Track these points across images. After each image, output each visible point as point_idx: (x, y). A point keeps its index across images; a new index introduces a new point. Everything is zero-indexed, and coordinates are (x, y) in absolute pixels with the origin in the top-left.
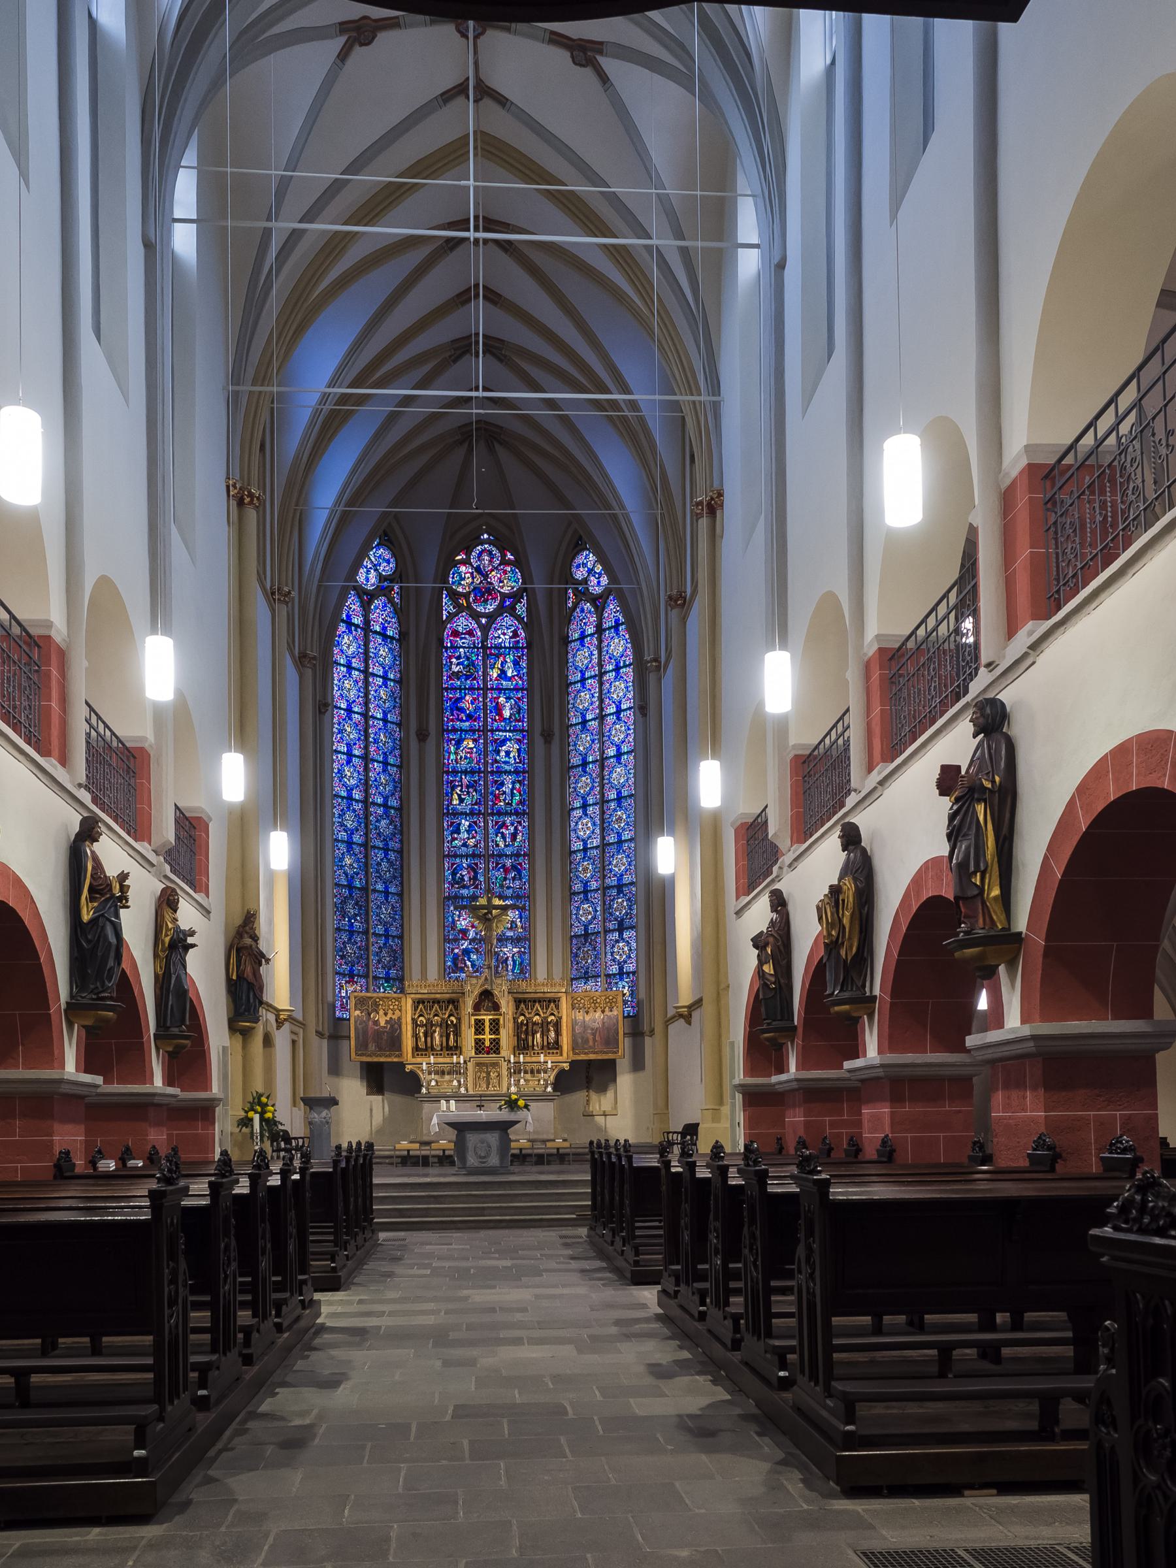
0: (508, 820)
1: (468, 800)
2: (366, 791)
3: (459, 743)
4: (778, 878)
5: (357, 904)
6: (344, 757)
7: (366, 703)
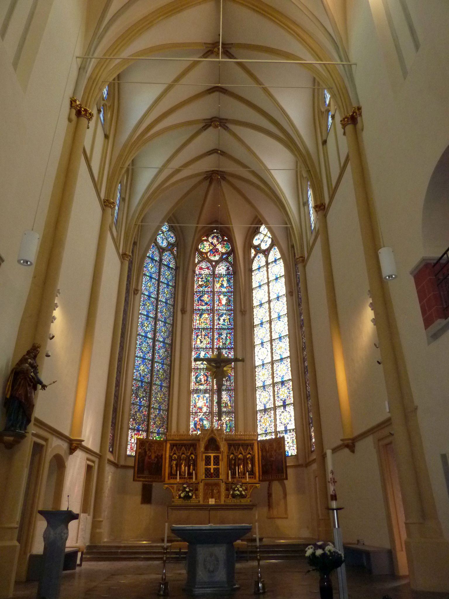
1: (205, 342)
2: (155, 334)
3: (201, 316)
5: (144, 391)
6: (145, 317)
7: (158, 294)
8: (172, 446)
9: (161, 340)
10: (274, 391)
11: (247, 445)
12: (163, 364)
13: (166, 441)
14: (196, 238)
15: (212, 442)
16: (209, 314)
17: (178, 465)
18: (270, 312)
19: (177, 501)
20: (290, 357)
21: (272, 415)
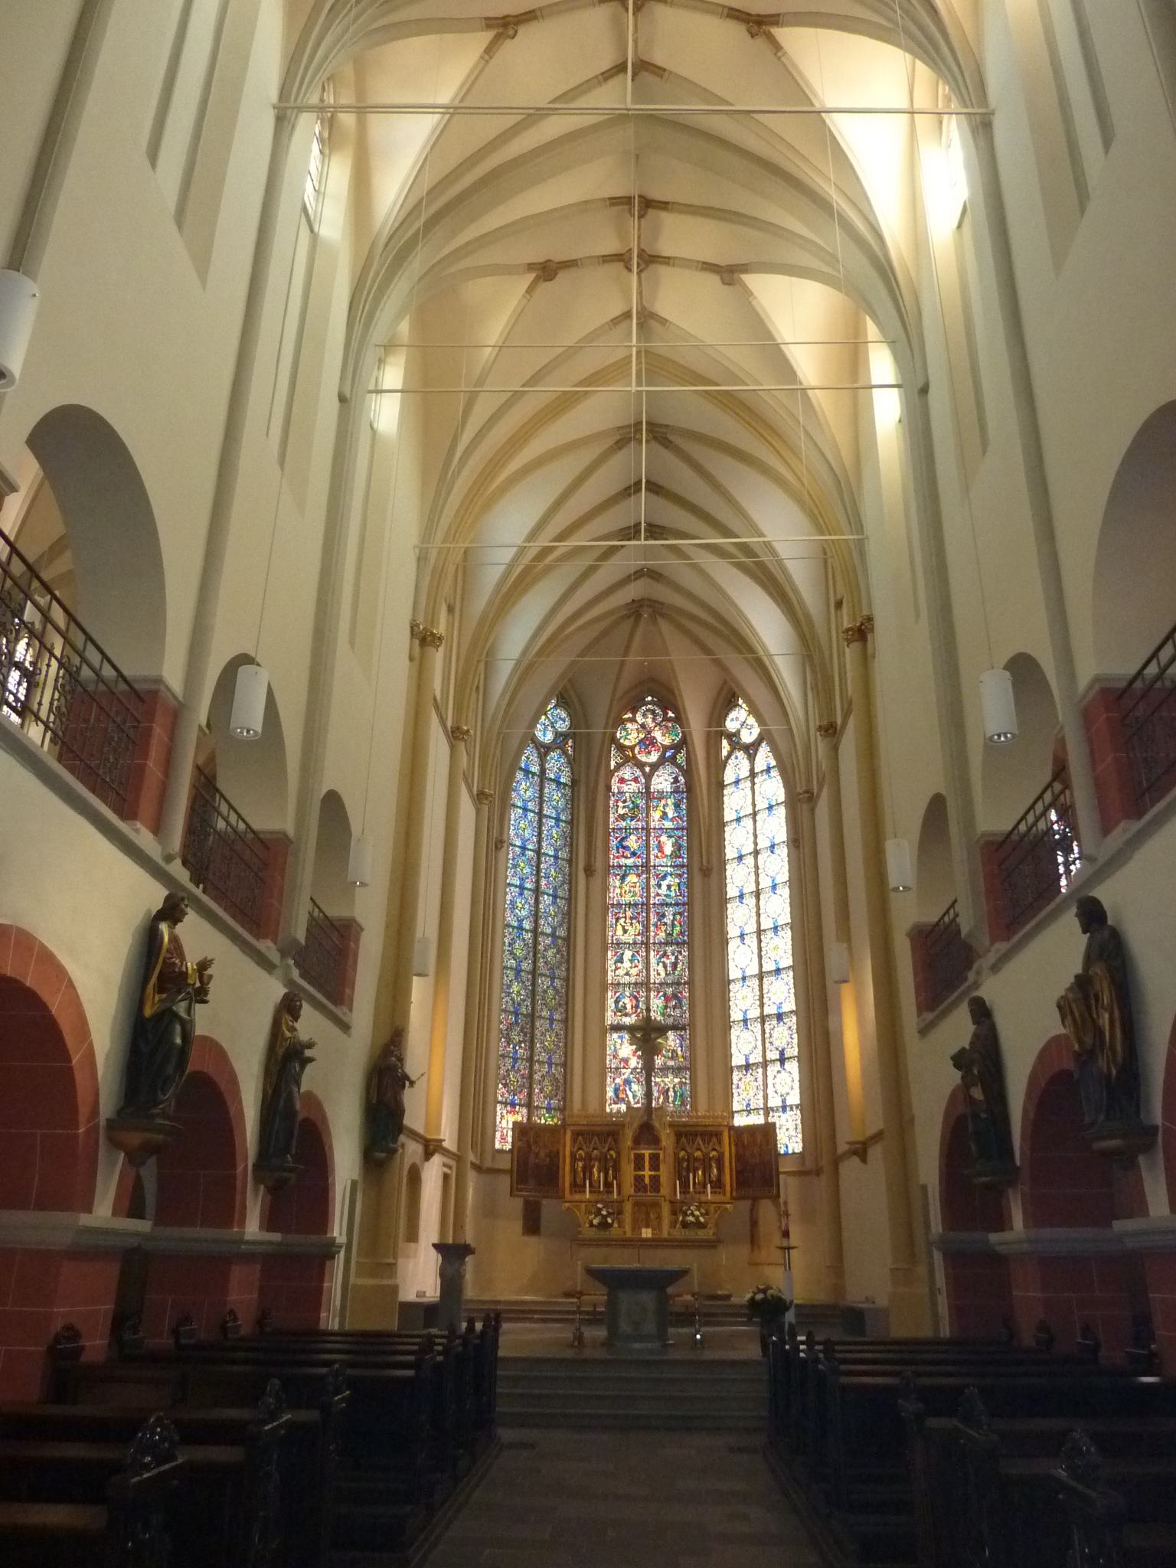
0: (669, 949)
2: (536, 922)
3: (623, 878)
4: (976, 985)
7: (539, 842)
8: (576, 1135)
9: (549, 931)
10: (763, 1032)
11: (711, 1135)
12: (553, 979)
13: (564, 1126)
14: (613, 715)
15: (646, 1125)
16: (639, 875)
17: (588, 1169)
18: (757, 875)
19: (588, 1233)
20: (793, 967)
21: (760, 1076)
